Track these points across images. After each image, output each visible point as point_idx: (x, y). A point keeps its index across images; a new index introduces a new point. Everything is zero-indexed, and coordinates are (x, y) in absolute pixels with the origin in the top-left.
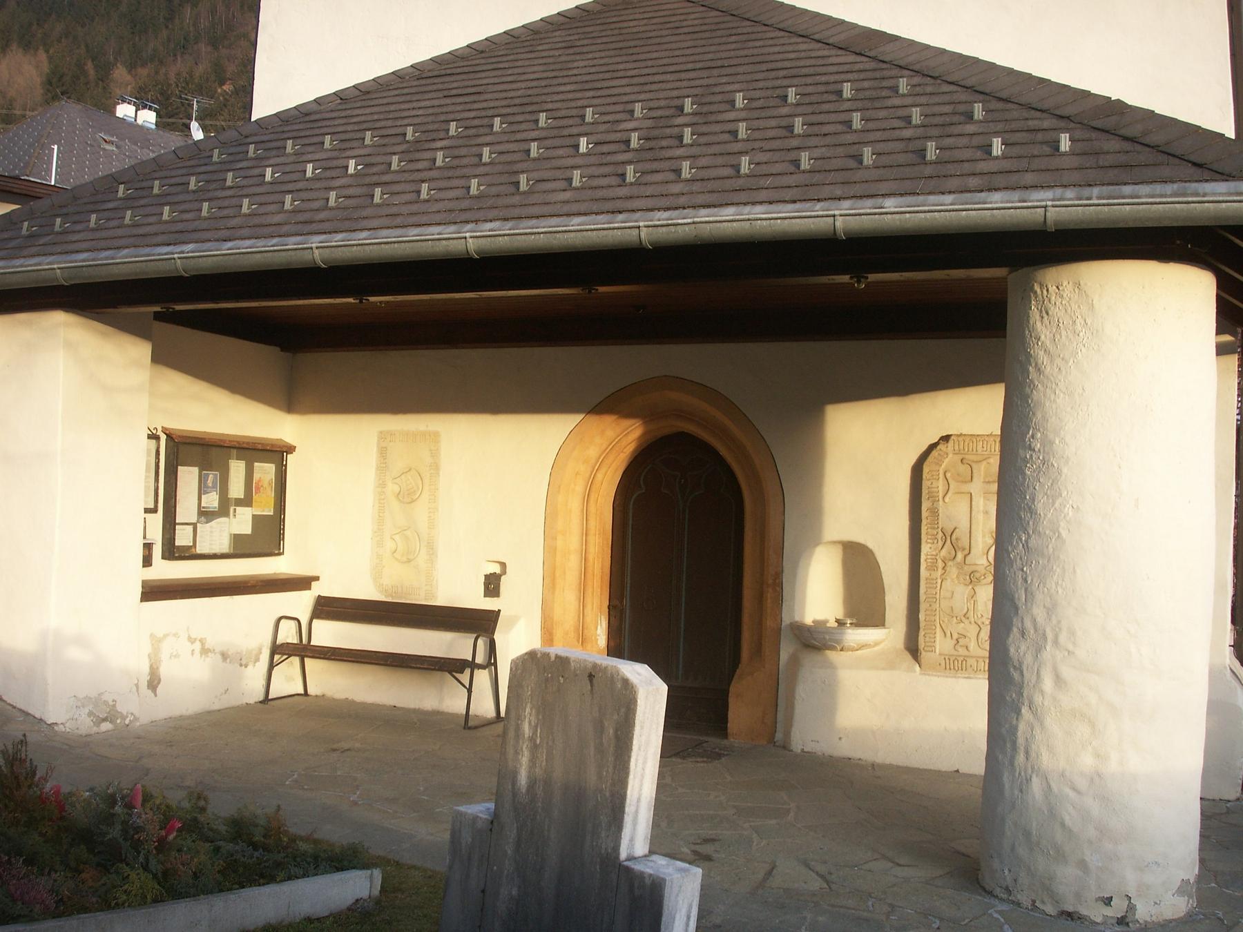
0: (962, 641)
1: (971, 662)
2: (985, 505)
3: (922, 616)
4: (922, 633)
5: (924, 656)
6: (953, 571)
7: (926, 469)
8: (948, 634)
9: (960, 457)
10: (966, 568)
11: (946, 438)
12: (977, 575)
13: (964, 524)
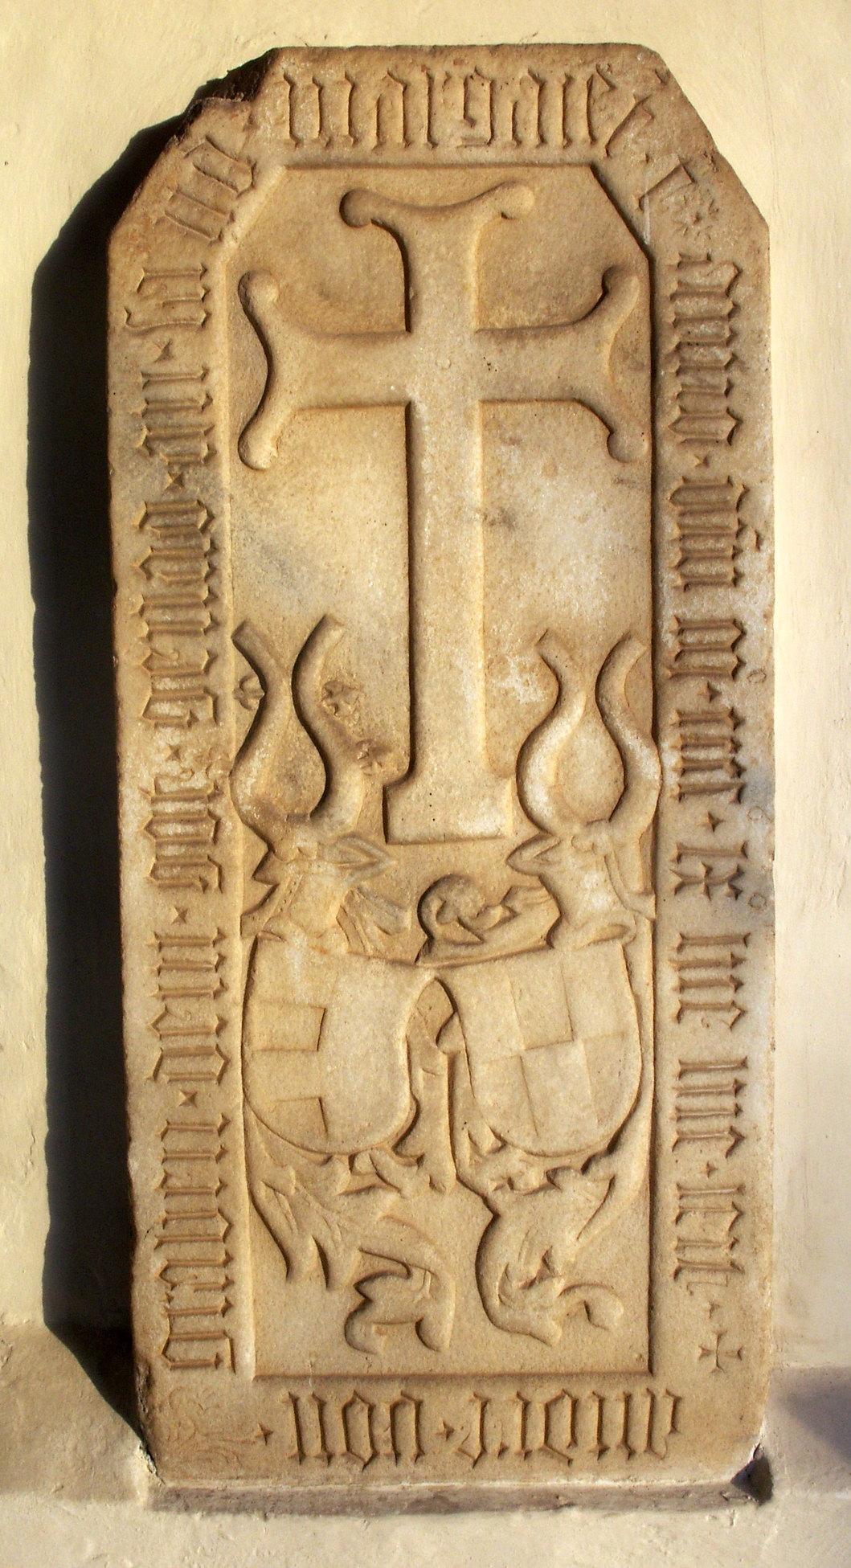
0: (389, 1296)
1: (453, 1408)
2: (496, 474)
3: (145, 1165)
4: (149, 1262)
5: (174, 1390)
6: (320, 886)
7: (126, 264)
8: (308, 1261)
9: (334, 183)
10: (395, 862)
11: (245, 82)
12: (466, 902)
13: (371, 589)
